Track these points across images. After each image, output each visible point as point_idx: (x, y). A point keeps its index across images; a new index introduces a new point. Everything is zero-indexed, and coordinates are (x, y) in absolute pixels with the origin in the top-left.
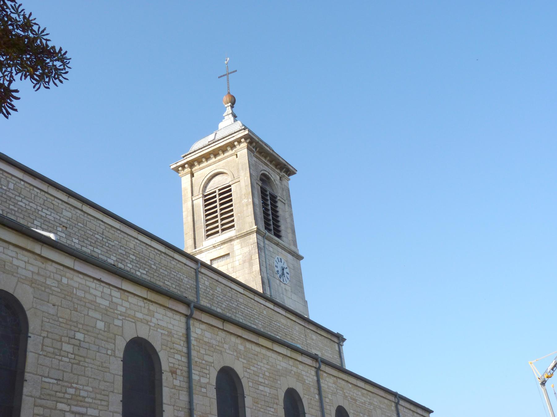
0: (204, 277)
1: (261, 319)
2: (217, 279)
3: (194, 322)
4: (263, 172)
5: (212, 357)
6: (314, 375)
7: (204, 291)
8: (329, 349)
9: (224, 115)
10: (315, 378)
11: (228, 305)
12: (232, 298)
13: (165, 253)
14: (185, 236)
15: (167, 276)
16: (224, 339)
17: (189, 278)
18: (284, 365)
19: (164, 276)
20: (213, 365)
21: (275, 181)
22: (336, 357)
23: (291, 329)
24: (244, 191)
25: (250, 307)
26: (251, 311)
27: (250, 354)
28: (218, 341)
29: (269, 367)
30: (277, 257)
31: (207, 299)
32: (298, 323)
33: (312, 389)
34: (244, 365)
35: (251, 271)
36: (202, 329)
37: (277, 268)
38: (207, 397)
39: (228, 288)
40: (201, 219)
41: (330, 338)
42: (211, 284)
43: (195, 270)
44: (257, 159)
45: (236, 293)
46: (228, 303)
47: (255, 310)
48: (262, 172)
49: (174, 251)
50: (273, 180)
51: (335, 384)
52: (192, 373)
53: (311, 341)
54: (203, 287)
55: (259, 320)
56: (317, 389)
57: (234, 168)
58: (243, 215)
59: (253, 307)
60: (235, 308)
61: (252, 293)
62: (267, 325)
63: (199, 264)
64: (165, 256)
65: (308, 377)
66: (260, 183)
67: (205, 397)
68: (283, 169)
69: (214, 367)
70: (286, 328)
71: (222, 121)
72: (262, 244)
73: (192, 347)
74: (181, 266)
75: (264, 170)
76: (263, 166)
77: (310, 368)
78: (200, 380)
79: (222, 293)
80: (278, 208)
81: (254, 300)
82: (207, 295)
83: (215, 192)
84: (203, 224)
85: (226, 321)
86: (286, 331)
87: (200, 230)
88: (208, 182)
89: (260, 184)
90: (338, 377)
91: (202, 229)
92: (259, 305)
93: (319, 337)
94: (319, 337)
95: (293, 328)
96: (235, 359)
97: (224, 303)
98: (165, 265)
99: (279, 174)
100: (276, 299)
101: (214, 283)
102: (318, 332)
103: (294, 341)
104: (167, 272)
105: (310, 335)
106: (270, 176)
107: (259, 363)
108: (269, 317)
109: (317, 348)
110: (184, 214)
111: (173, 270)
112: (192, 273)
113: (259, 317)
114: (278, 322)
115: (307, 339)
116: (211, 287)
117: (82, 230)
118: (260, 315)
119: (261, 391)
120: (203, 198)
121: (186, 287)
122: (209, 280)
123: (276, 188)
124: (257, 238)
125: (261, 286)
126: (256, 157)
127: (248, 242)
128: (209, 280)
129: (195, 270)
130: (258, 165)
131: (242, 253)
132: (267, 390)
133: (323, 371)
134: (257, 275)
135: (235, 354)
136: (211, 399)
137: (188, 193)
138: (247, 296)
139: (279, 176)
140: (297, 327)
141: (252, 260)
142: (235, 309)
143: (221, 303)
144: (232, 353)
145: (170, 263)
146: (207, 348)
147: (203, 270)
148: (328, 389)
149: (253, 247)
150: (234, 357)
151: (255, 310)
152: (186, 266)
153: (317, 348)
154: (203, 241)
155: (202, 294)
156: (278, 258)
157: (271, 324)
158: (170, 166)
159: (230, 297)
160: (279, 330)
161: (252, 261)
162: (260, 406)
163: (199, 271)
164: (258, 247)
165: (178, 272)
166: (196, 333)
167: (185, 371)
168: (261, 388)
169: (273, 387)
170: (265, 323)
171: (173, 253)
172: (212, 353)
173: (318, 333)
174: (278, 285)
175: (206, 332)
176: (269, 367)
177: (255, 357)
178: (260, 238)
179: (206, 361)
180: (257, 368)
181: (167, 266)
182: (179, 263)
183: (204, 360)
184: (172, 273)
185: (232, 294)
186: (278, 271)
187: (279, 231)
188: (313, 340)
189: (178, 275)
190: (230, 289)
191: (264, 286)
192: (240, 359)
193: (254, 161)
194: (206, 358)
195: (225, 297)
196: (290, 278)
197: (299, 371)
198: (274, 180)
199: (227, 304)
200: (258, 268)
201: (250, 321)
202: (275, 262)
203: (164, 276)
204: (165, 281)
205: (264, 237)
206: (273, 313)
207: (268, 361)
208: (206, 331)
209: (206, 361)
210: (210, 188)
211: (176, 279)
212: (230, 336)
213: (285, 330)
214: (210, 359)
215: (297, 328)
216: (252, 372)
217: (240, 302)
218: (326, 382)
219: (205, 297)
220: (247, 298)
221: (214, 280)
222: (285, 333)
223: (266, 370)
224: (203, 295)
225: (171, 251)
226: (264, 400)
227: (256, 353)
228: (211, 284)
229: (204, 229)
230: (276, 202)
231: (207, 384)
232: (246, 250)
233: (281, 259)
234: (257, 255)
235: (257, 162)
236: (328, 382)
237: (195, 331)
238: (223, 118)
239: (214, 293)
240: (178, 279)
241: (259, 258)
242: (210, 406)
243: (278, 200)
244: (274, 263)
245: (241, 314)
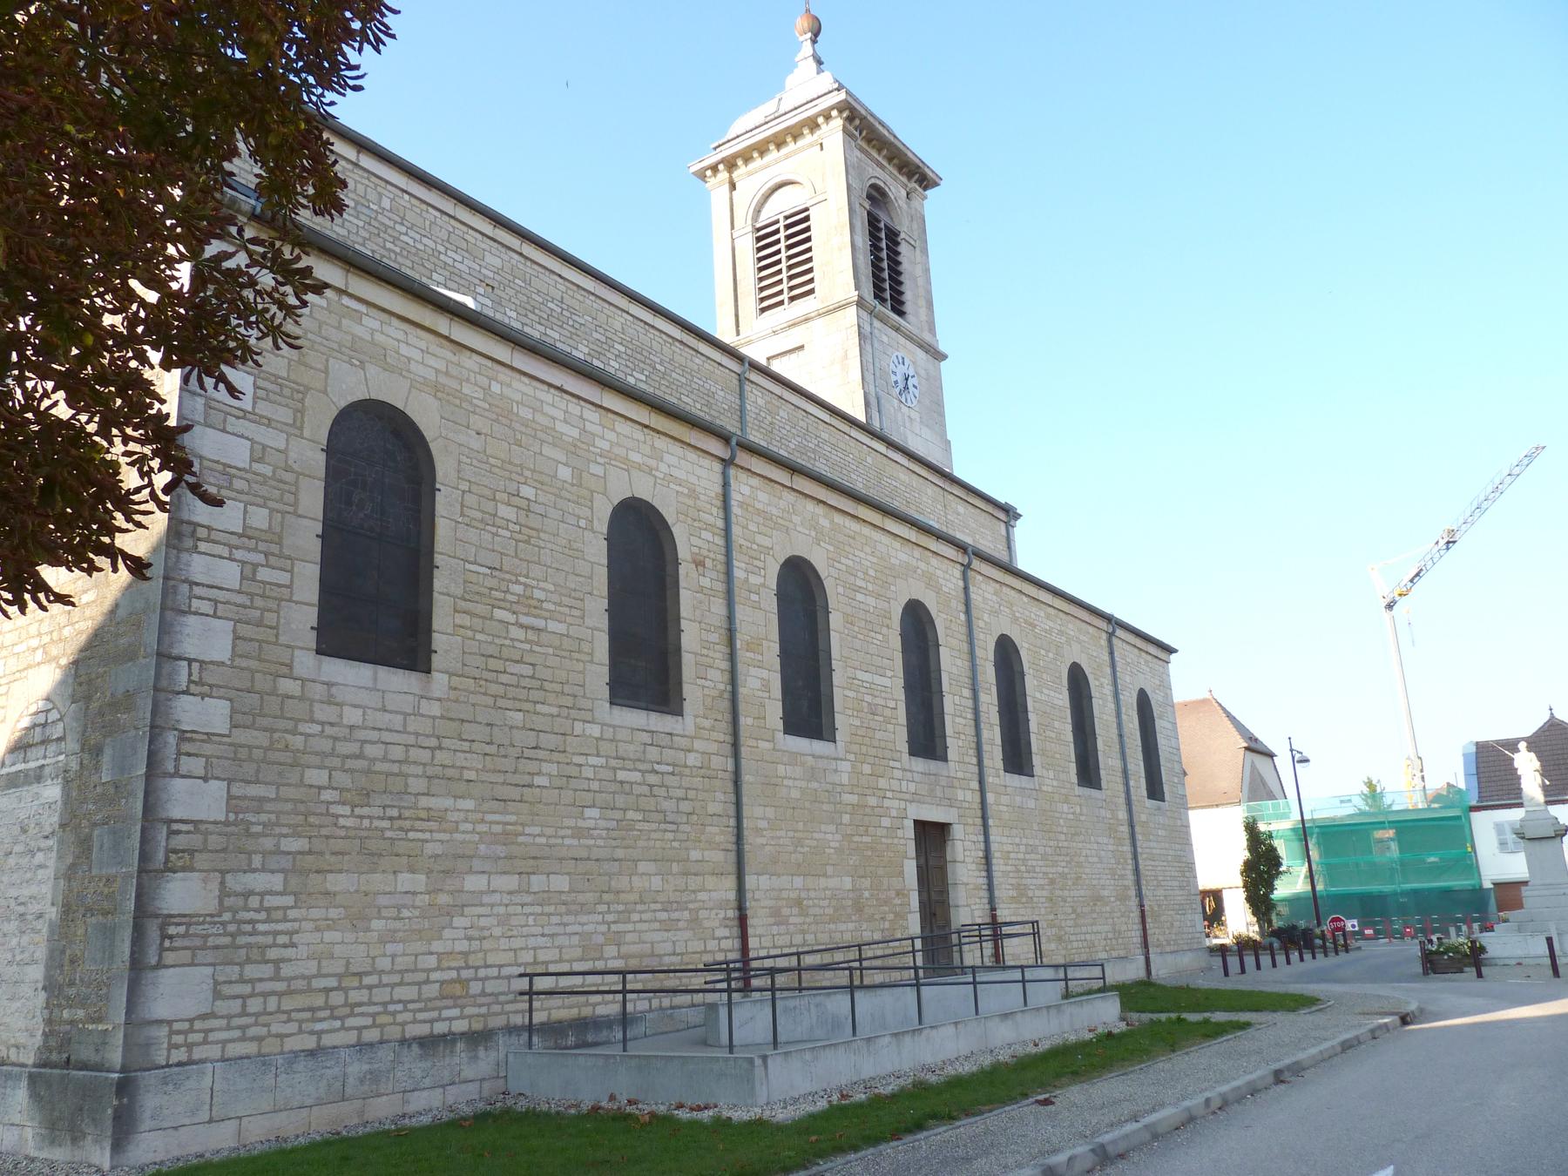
4: (873, 181)
10: (961, 583)
29: (875, 560)
34: (680, 499)
60: (814, 451)
66: (867, 204)
72: (867, 328)
73: (734, 519)
83: (777, 222)
105: (954, 505)
107: (857, 553)
126: (862, 150)
132: (871, 601)
135: (813, 534)
168: (860, 597)
178: (865, 315)
186: (896, 382)
188: (958, 514)
194: (759, 539)
214: (767, 542)
215: (929, 492)
216: (844, 568)
238: (795, 65)
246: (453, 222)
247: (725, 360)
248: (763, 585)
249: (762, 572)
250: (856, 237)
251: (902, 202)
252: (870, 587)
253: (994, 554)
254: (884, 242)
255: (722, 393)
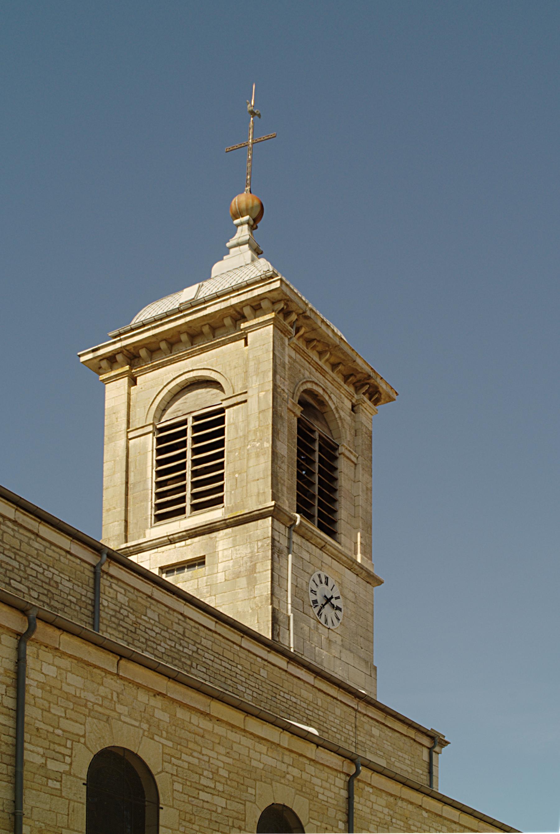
0: (116, 585)
1: (253, 684)
2: (149, 594)
3: (39, 649)
4: (309, 386)
5: (81, 724)
6: (343, 787)
7: (114, 613)
8: (406, 757)
9: (228, 245)
10: (344, 793)
11: (173, 649)
12: (184, 635)
13: (15, 522)
14: (104, 515)
15: (16, 570)
16: (118, 694)
17: (76, 582)
18: (271, 762)
19: (10, 571)
20: (82, 740)
21: (337, 411)
22: (421, 772)
23: (323, 712)
24: (254, 424)
25: (229, 659)
26: (229, 667)
27: (183, 731)
28: (102, 697)
29: (230, 761)
30: (320, 572)
31: (120, 631)
32: (341, 702)
33: (332, 812)
34: (166, 751)
35: (251, 595)
36: (59, 668)
37: (316, 594)
38: (61, 797)
39: (175, 614)
40: (145, 481)
41: (414, 737)
42: (134, 601)
43: (94, 567)
44: (298, 355)
45: (195, 627)
46: (173, 645)
47: (239, 666)
48: (305, 387)
49: (39, 520)
50: (333, 407)
51: (389, 809)
52: (23, 748)
53: (368, 737)
54: (111, 605)
55: (247, 686)
56: (344, 813)
57: (236, 369)
58: (247, 476)
59: (237, 660)
60: (190, 657)
61: (236, 631)
62: (267, 698)
63: (105, 556)
64: (16, 528)
65: (325, 788)
66: (298, 410)
67: (58, 798)
68: (363, 385)
69: (85, 744)
70: (311, 708)
71: (222, 259)
72: (284, 542)
73: (28, 698)
74: (56, 554)
75: (313, 382)
76: (310, 373)
77: (335, 773)
78: (46, 764)
79: (159, 622)
80: (339, 470)
81: (240, 646)
82: (121, 623)
83: (185, 422)
84: (150, 491)
85: (125, 657)
86: (310, 713)
87: (142, 504)
88: (169, 399)
89: (299, 413)
90: (400, 797)
91: (146, 500)
92: (251, 658)
93: (388, 733)
94: (388, 733)
95: (327, 710)
96: (144, 735)
97: (162, 644)
98: (14, 548)
99: (350, 397)
100: (302, 655)
101: (140, 599)
102: (386, 724)
103: (327, 734)
104: (18, 562)
105: (367, 727)
106: (327, 398)
107: (205, 751)
108: (272, 684)
109: (378, 752)
110: (107, 467)
111: (33, 560)
112: (84, 573)
113: (248, 681)
114: (294, 695)
115: (358, 733)
116: (132, 609)
117: (109, 616)
118: (251, 678)
119: (204, 801)
120: (154, 433)
121: (67, 599)
122: (129, 592)
123: (339, 427)
124: (272, 528)
125: (270, 625)
126: (296, 349)
127: (250, 535)
128: (129, 592)
129: (94, 567)
130: (299, 367)
131: (233, 558)
132: (221, 802)
133: (365, 782)
134: (264, 603)
135: (145, 726)
136: (72, 804)
137: (119, 420)
138: (224, 637)
139: (351, 401)
140: (339, 710)
141: (255, 573)
142: (189, 659)
143: (154, 642)
144: (137, 724)
145: (29, 544)
146: (71, 706)
147: (114, 570)
148: (372, 815)
149: (262, 546)
150: (141, 731)
151: (239, 666)
152: (69, 556)
153: (378, 752)
154: (147, 528)
155: (109, 618)
156: (319, 576)
157: (276, 697)
158: (80, 356)
159: (179, 633)
160: (295, 710)
161: (255, 575)
162: (196, 827)
163: (103, 571)
164: (273, 546)
165: (48, 566)
166: (43, 673)
167: (6, 744)
168: (203, 796)
169: (234, 797)
170: (260, 693)
171: (37, 524)
172: (84, 717)
173: (386, 726)
174: (313, 628)
175: (69, 674)
176: (230, 761)
177: (198, 738)
178: (282, 528)
179: (64, 731)
180: (198, 759)
181: (17, 550)
182: (53, 547)
183: (61, 729)
184: (32, 565)
185: (184, 628)
186: (315, 602)
187: (334, 522)
188: (372, 736)
189: (46, 573)
190: (181, 617)
191: (278, 627)
192: (156, 737)
193: (290, 357)
194: (65, 724)
195: (167, 631)
196: (343, 619)
197: (305, 776)
198: (336, 408)
199: (171, 646)
200: (268, 589)
201: (225, 686)
202: (311, 582)
203: (10, 571)
204: (12, 581)
205: (291, 527)
206: (329, 701)
207: (228, 750)
208: (70, 672)
209: (64, 731)
210: (175, 412)
211: (40, 580)
212: (135, 691)
213: (307, 711)
214: (77, 729)
215: (338, 712)
216: (186, 765)
217: (203, 646)
218: (369, 804)
219: (114, 626)
220: (223, 640)
221: (141, 594)
222: (307, 718)
223: (221, 765)
224: (111, 621)
225: (31, 518)
226: (208, 819)
227: (201, 731)
228: (134, 601)
229: (150, 503)
230: (336, 458)
231: (64, 775)
232: (244, 551)
233: (327, 578)
234: (269, 562)
235: (297, 360)
236: (373, 802)
237: (39, 669)
238: (227, 251)
239: (139, 621)
240: (47, 581)
241: (272, 570)
242: (68, 815)
243: (340, 454)
244: (308, 584)
245: (204, 670)
246: (215, 635)
247: (77, 549)
248: (69, 773)
249: (68, 759)
250: (279, 444)
251: (345, 414)
252: (220, 787)
253: (411, 777)
254: (317, 454)
255: (70, 585)
